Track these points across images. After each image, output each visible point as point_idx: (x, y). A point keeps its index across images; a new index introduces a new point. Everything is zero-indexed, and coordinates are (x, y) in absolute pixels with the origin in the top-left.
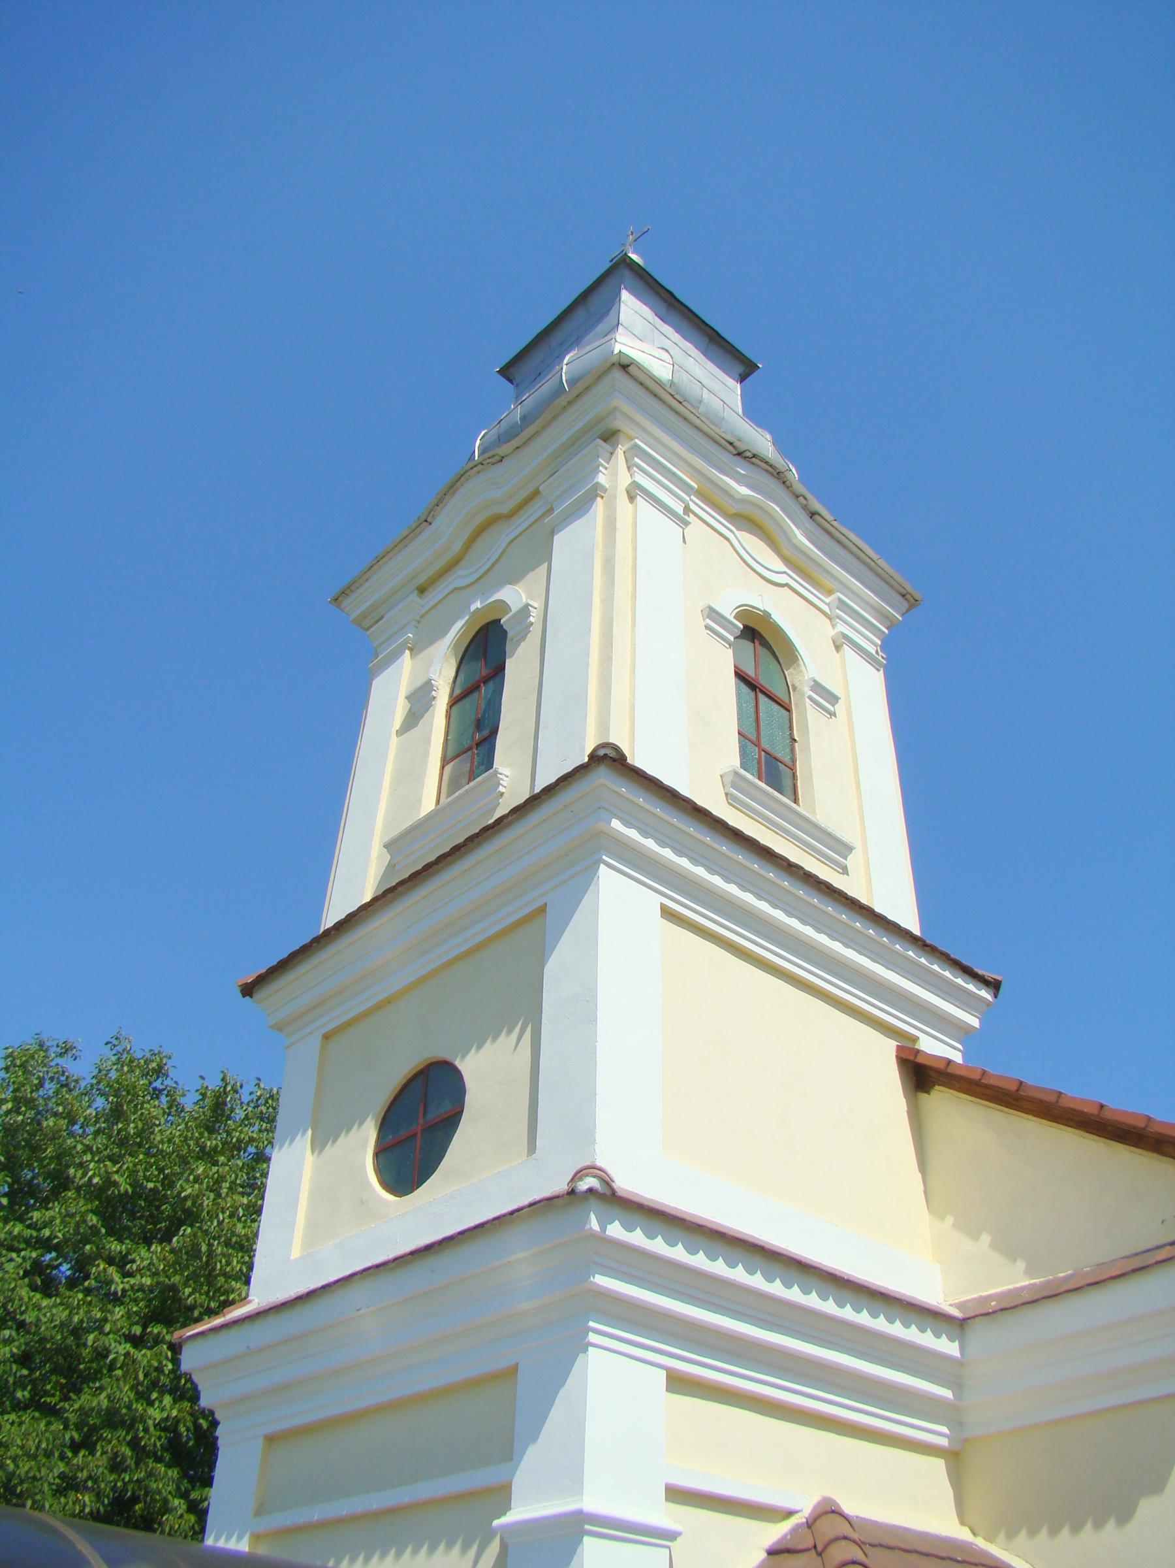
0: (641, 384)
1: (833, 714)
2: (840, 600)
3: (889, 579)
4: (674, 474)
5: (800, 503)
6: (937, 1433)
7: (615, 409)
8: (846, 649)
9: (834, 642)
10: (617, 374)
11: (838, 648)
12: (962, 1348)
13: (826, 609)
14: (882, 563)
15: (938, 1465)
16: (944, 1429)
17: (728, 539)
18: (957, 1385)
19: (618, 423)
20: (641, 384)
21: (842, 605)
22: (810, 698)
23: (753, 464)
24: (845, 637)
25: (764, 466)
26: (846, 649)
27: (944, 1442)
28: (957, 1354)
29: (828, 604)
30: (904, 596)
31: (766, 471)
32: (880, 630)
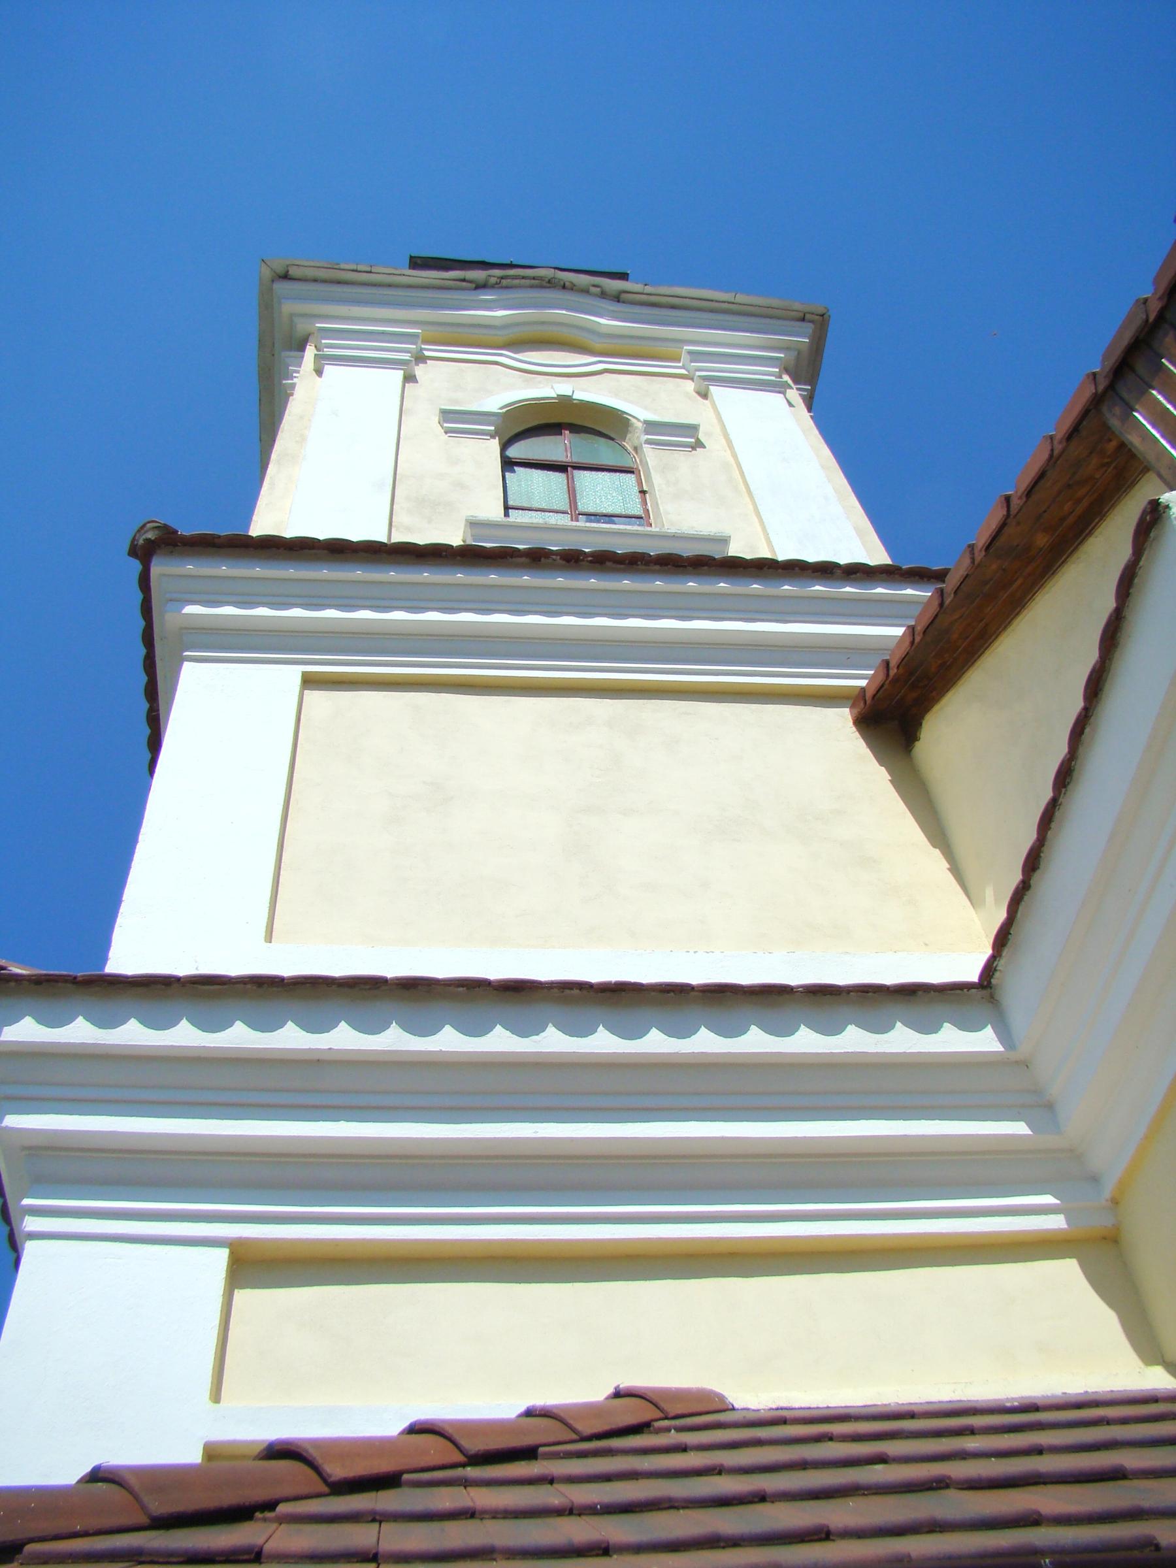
0: (315, 280)
1: (699, 444)
2: (690, 353)
3: (770, 312)
4: (383, 333)
5: (595, 295)
6: (1040, 1213)
7: (292, 315)
8: (714, 390)
9: (699, 393)
10: (281, 287)
11: (704, 395)
12: (1004, 1034)
13: (683, 371)
14: (741, 298)
15: (1066, 1272)
16: (1048, 1199)
17: (496, 363)
18: (1039, 1106)
19: (302, 327)
20: (315, 280)
21: (695, 356)
22: (648, 442)
23: (507, 287)
24: (705, 378)
25: (528, 282)
26: (714, 390)
27: (1056, 1222)
28: (997, 1047)
29: (683, 367)
30: (803, 320)
31: (532, 287)
32: (771, 358)
